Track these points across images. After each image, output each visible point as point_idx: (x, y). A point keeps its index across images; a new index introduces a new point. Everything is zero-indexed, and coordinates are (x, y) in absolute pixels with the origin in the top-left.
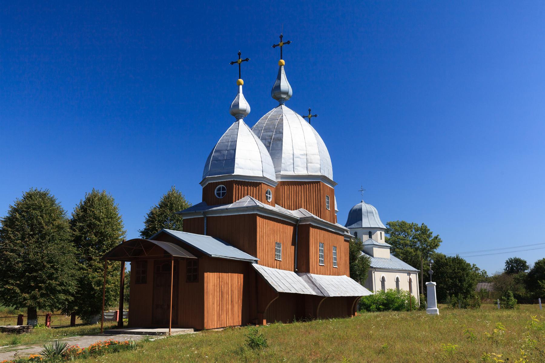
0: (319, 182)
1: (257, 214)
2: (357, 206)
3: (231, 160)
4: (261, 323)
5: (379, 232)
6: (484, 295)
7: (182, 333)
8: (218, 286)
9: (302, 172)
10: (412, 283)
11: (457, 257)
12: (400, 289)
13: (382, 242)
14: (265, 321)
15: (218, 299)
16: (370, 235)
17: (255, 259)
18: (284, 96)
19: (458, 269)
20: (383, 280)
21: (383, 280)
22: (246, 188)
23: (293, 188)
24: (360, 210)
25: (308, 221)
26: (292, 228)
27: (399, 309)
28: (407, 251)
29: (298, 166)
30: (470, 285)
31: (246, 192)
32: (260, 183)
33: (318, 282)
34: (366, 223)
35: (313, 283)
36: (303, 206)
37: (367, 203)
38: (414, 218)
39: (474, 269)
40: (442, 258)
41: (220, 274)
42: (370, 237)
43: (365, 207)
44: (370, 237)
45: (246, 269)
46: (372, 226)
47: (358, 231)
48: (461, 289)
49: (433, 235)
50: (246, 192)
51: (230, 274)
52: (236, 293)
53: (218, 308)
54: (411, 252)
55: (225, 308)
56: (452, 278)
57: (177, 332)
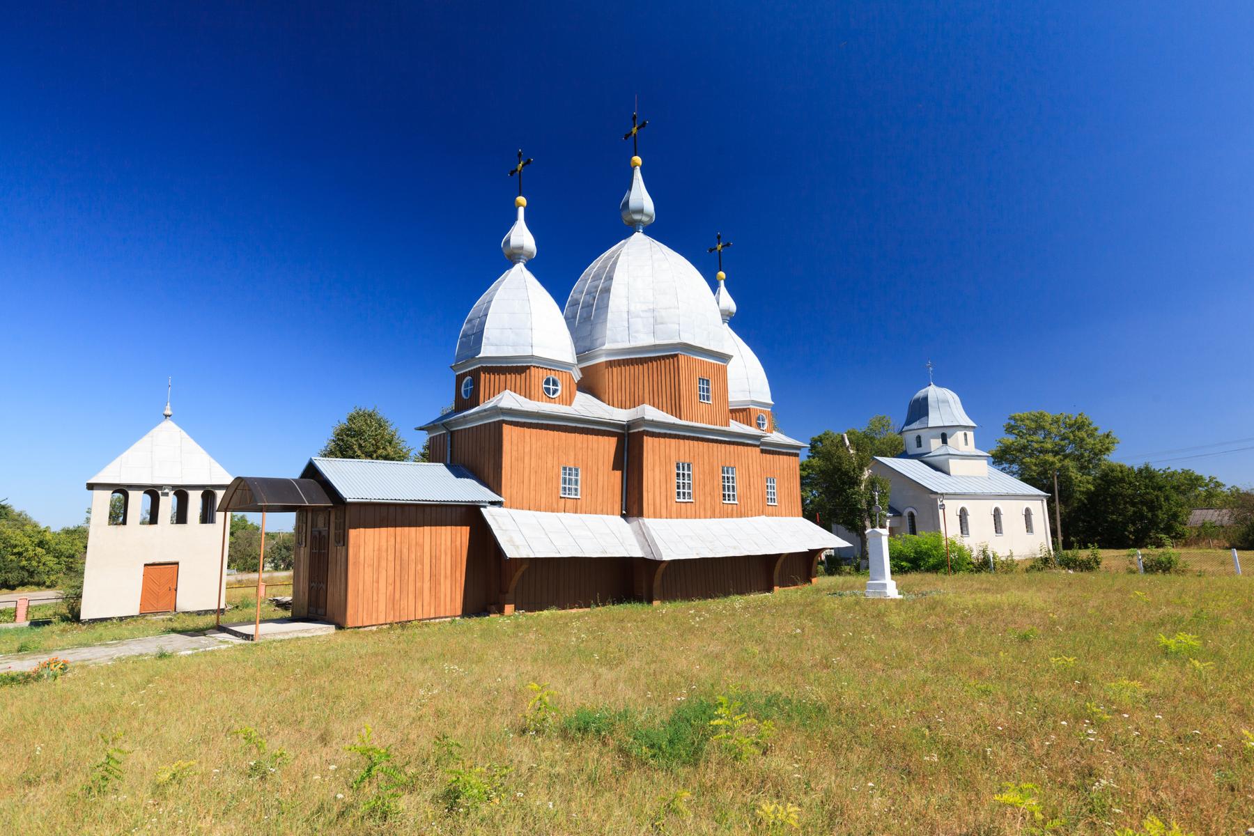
0: (676, 355)
1: (504, 421)
2: (921, 394)
3: (477, 337)
4: (501, 611)
5: (960, 434)
6: (1204, 535)
7: (319, 633)
8: (391, 552)
9: (644, 340)
10: (1033, 517)
11: (1147, 468)
12: (136, 612)
13: (971, 448)
14: (509, 608)
15: (391, 572)
16: (944, 439)
17: (496, 498)
18: (637, 217)
19: (1147, 487)
20: (963, 515)
21: (963, 515)
22: (502, 377)
23: (627, 370)
24: (926, 399)
25: (640, 426)
26: (614, 440)
27: (935, 569)
28: (1046, 462)
29: (637, 332)
30: (1175, 516)
31: (503, 385)
32: (528, 367)
33: (653, 533)
34: (934, 419)
35: (644, 537)
36: (647, 400)
37: (939, 384)
38: (1056, 406)
39: (1212, 485)
40: (1113, 471)
41: (398, 529)
42: (945, 441)
43: (934, 392)
44: (945, 441)
45: (470, 515)
46: (947, 424)
47: (922, 433)
48: (1153, 523)
49: (1100, 433)
50: (503, 385)
51: (427, 529)
52: (446, 562)
53: (391, 588)
54: (1052, 463)
55: (411, 588)
56: (1134, 504)
57: (307, 631)
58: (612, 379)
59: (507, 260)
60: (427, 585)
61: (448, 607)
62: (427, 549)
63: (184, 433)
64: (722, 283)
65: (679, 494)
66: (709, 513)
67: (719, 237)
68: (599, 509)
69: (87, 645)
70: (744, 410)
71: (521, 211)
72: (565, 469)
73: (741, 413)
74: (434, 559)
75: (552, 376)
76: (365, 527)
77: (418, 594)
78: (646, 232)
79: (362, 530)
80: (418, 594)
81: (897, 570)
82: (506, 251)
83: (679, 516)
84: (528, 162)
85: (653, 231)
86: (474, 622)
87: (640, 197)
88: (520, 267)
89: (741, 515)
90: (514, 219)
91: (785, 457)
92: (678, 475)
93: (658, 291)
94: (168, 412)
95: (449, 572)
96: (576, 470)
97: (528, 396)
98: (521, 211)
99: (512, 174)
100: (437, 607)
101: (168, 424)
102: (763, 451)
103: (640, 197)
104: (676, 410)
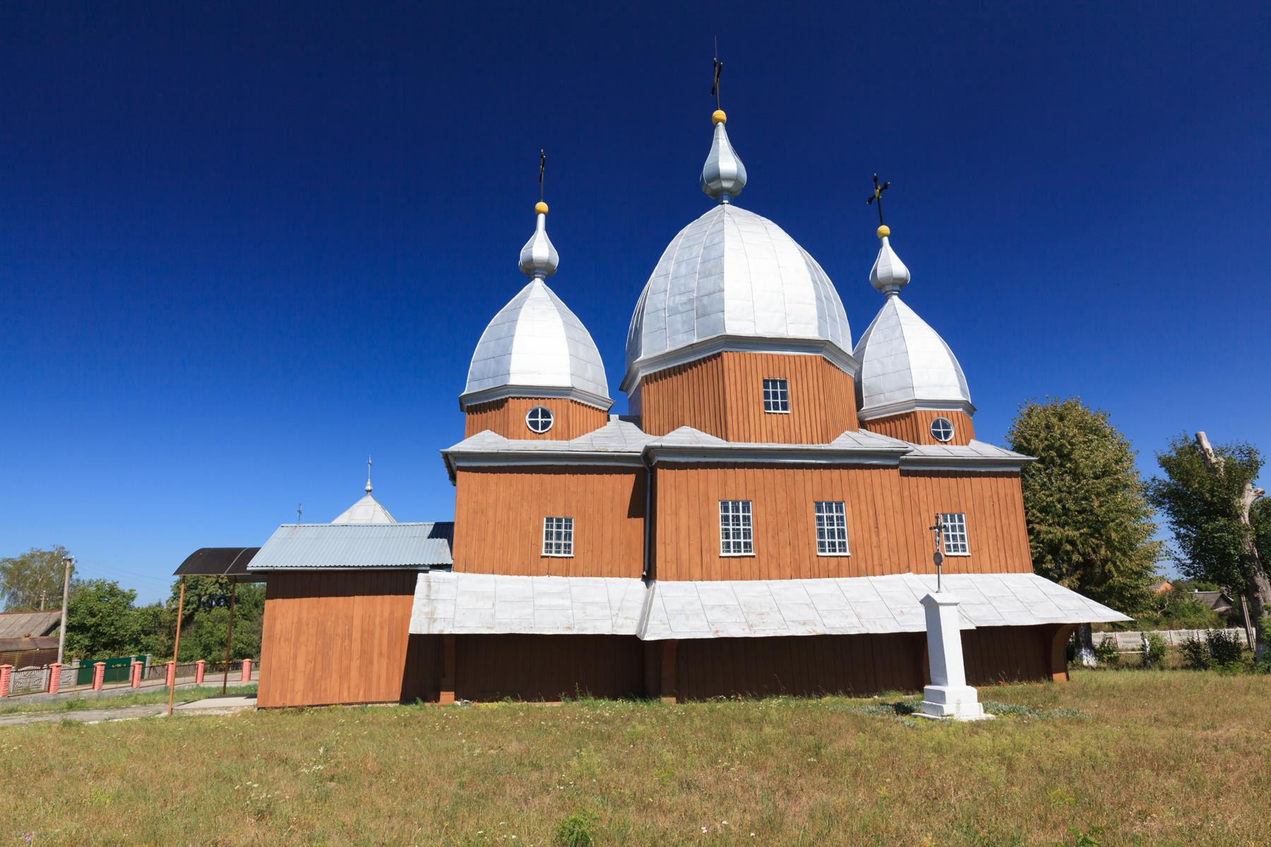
0: (720, 354)
18: (714, 185)
23: (675, 380)
32: (506, 400)
58: (651, 398)
59: (521, 276)
60: (355, 664)
61: (382, 691)
62: (357, 622)
63: (378, 506)
64: (886, 240)
65: (822, 544)
66: (894, 568)
67: (876, 179)
68: (903, 566)
69: (118, 708)
70: (908, 415)
71: (541, 219)
72: (550, 520)
73: (900, 421)
74: (368, 633)
75: (540, 405)
76: (283, 598)
77: (344, 675)
78: (734, 202)
79: (279, 601)
80: (344, 675)
81: (973, 677)
82: (874, 284)
83: (726, 576)
84: (886, 186)
85: (752, 197)
86: (409, 709)
87: (725, 160)
88: (538, 283)
89: (857, 571)
90: (880, 245)
91: (986, 480)
92: (726, 519)
93: (748, 273)
94: (369, 488)
95: (385, 649)
96: (569, 520)
97: (507, 435)
98: (541, 219)
99: (870, 201)
100: (378, 694)
101: (369, 499)
102: (904, 474)
103: (725, 160)
104: (723, 433)
